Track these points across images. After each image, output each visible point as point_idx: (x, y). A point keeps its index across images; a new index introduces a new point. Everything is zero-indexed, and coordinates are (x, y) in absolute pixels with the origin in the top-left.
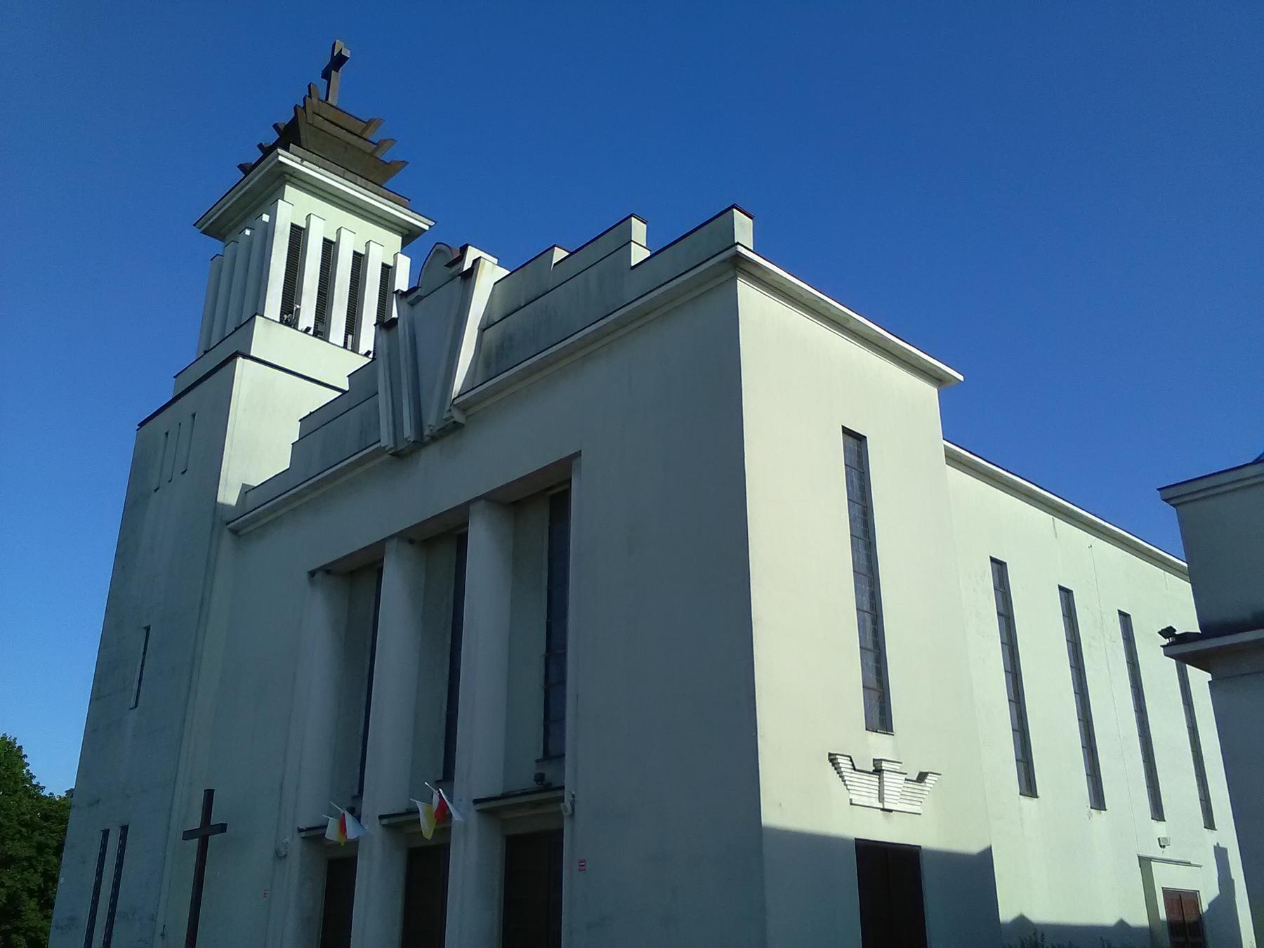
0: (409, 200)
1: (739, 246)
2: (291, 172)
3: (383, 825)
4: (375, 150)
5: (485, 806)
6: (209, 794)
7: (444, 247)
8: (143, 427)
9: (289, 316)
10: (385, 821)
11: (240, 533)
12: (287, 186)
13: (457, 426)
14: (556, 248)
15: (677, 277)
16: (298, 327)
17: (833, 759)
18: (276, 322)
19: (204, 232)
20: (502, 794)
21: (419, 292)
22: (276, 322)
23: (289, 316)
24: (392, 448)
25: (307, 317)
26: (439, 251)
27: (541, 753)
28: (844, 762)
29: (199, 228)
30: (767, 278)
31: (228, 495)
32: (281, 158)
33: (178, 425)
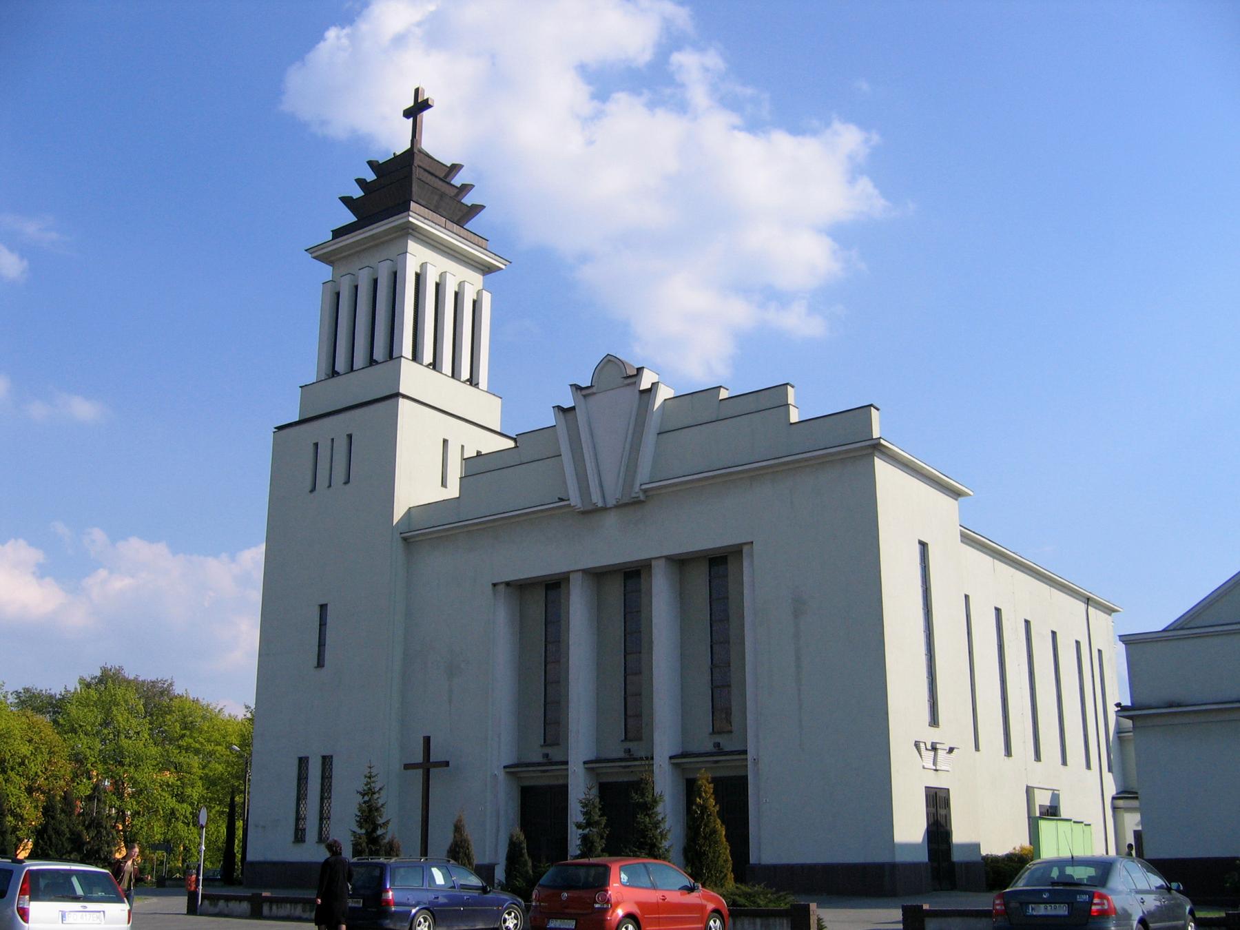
0: (511, 263)
1: (881, 440)
2: (414, 228)
3: (586, 768)
4: (457, 195)
5: (590, 765)
6: (427, 740)
7: (613, 359)
8: (280, 432)
9: (416, 357)
10: (508, 770)
11: (408, 541)
12: (409, 241)
13: (641, 502)
14: (722, 389)
15: (838, 446)
16: (423, 362)
17: (917, 745)
18: (448, 376)
19: (315, 258)
20: (682, 753)
21: (594, 390)
22: (448, 376)
23: (416, 357)
24: (580, 508)
25: (428, 357)
26: (609, 361)
27: (711, 731)
28: (922, 745)
29: (311, 253)
30: (889, 453)
31: (399, 512)
32: (411, 219)
33: (330, 440)
